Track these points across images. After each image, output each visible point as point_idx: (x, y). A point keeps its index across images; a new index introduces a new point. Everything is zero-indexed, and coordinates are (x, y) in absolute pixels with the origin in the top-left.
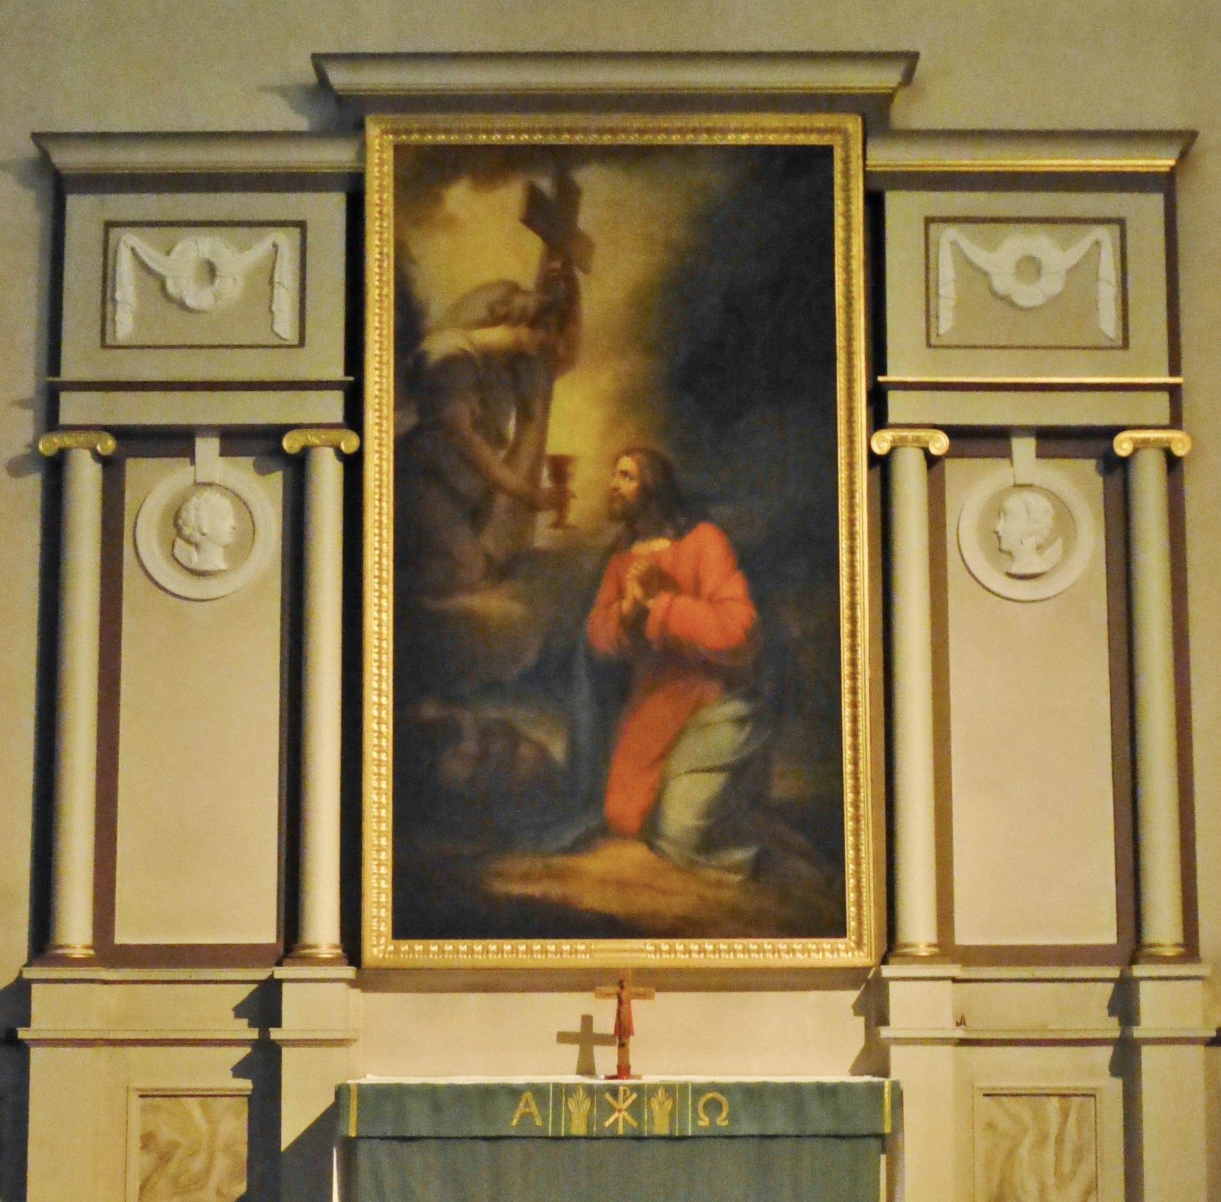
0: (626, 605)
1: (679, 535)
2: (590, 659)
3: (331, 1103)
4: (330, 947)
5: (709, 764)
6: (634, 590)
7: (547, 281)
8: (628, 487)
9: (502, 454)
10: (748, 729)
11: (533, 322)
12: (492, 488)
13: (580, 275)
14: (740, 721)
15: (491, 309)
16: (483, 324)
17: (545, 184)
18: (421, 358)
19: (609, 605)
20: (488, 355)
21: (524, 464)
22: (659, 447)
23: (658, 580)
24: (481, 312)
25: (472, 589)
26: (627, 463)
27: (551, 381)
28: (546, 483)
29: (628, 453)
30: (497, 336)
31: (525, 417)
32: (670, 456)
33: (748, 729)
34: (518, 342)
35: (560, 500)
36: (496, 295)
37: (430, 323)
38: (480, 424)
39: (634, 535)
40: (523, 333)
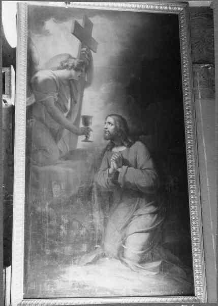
0: (111, 170)
1: (129, 146)
2: (98, 189)
3: (11, 45)
4: (10, 98)
5: (142, 230)
6: (113, 165)
7: (81, 55)
8: (111, 128)
9: (66, 114)
10: (156, 216)
11: (77, 69)
12: (63, 126)
13: (93, 53)
14: (153, 214)
15: (62, 64)
16: (59, 69)
17: (81, 22)
18: (36, 83)
19: (104, 170)
20: (60, 80)
21: (74, 118)
22: (120, 114)
23: (123, 162)
24: (58, 65)
25: (56, 164)
26: (111, 119)
27: (83, 90)
28: (81, 125)
29: (110, 116)
30: (64, 73)
31: (74, 102)
32: (126, 118)
33: (156, 216)
34: (71, 76)
35: (86, 132)
36: (64, 58)
37: (38, 67)
38: (57, 103)
39: (113, 145)
40: (73, 72)
